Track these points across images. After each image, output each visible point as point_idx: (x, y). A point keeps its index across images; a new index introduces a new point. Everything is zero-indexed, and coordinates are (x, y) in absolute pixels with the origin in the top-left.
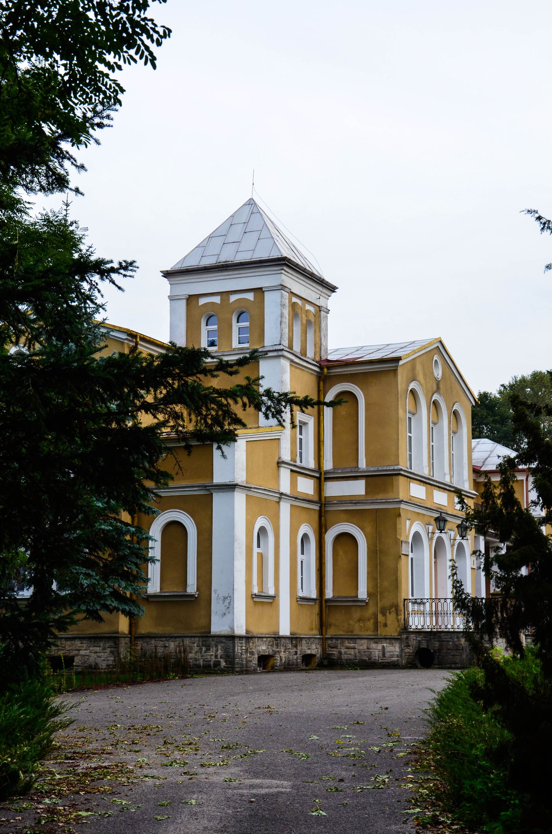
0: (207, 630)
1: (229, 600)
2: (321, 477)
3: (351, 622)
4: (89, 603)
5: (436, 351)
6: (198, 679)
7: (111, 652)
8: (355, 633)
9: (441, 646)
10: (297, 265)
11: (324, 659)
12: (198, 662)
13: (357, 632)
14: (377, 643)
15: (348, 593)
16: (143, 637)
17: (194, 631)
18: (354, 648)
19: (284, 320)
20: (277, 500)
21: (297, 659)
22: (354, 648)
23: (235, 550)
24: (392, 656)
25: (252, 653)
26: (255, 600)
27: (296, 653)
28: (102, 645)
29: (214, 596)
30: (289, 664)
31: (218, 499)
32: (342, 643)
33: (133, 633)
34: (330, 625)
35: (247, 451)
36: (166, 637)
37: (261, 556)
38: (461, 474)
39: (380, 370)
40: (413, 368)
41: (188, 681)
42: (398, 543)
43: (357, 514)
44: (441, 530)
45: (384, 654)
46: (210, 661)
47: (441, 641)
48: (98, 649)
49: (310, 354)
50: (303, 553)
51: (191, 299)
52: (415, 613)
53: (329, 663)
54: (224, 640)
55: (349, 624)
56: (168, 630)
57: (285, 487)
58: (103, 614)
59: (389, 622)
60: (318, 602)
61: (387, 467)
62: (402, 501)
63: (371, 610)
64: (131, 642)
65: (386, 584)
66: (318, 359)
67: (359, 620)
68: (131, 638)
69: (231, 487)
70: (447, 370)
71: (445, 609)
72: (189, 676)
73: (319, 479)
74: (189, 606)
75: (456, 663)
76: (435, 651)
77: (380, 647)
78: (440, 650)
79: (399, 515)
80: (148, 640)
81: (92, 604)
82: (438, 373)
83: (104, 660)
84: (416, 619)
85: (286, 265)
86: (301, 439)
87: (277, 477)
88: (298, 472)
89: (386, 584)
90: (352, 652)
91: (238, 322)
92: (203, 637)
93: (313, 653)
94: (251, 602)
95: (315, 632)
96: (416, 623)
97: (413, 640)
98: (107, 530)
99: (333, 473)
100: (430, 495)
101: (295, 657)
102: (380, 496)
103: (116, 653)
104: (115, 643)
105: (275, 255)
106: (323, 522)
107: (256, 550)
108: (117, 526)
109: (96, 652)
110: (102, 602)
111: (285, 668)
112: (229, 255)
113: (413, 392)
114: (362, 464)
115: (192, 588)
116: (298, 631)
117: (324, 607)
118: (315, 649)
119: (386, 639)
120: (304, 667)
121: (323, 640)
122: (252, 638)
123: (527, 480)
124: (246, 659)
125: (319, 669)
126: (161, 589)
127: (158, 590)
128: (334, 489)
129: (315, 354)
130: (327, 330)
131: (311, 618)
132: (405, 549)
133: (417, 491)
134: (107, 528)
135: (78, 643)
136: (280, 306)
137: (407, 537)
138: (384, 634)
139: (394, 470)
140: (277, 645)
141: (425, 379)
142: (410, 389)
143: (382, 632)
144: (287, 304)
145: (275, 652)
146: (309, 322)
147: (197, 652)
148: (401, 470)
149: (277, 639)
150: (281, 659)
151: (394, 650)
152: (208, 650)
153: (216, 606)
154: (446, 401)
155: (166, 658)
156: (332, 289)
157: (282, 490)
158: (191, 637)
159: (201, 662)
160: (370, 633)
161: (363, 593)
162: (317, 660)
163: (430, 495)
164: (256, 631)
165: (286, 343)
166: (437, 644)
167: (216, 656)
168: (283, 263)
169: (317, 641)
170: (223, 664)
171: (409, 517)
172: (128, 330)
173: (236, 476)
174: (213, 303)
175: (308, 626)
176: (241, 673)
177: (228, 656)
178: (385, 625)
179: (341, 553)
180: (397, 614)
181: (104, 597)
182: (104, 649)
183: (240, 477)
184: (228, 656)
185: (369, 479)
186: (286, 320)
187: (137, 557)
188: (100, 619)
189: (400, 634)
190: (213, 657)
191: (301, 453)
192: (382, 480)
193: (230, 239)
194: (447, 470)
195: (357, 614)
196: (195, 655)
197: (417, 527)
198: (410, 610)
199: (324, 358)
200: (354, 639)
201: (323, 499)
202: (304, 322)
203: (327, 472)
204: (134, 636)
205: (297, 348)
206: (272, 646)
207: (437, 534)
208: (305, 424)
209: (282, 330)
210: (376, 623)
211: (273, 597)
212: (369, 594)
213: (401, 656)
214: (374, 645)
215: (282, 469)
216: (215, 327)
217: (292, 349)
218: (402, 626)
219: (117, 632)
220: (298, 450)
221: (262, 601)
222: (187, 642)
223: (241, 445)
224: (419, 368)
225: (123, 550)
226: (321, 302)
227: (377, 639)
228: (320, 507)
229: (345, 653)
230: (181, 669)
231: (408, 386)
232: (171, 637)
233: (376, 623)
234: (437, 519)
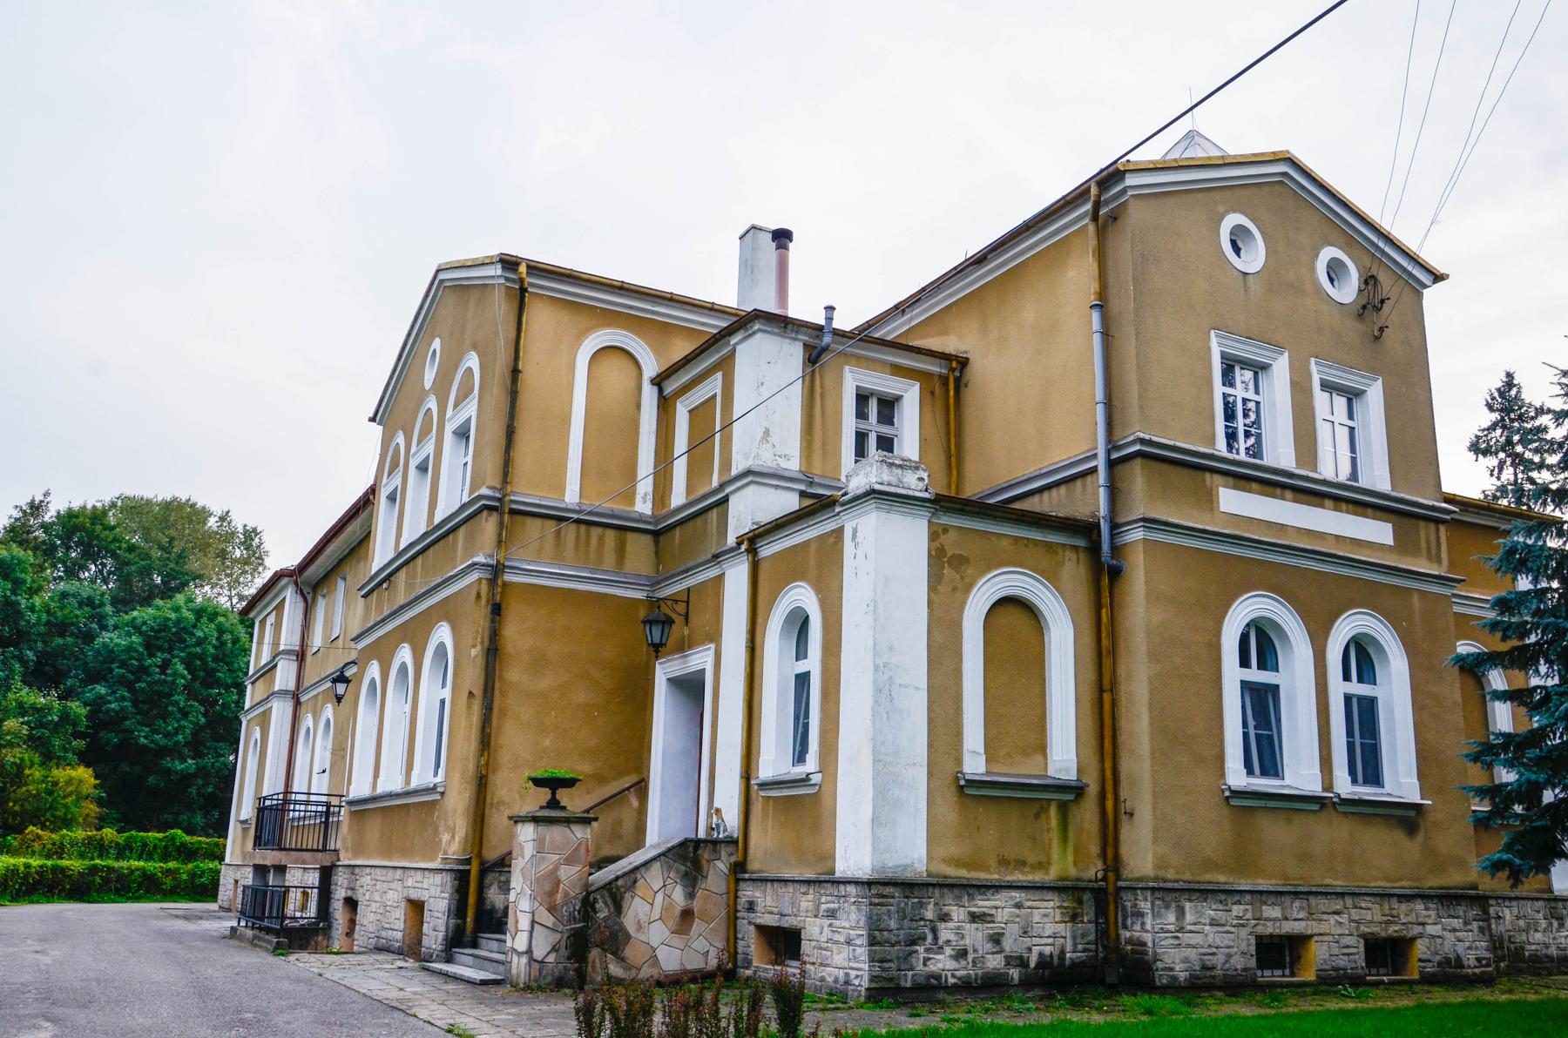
7: (1481, 930)
10: (732, 383)
48: (1456, 923)
83: (1470, 948)
135: (1419, 906)
159: (1553, 951)
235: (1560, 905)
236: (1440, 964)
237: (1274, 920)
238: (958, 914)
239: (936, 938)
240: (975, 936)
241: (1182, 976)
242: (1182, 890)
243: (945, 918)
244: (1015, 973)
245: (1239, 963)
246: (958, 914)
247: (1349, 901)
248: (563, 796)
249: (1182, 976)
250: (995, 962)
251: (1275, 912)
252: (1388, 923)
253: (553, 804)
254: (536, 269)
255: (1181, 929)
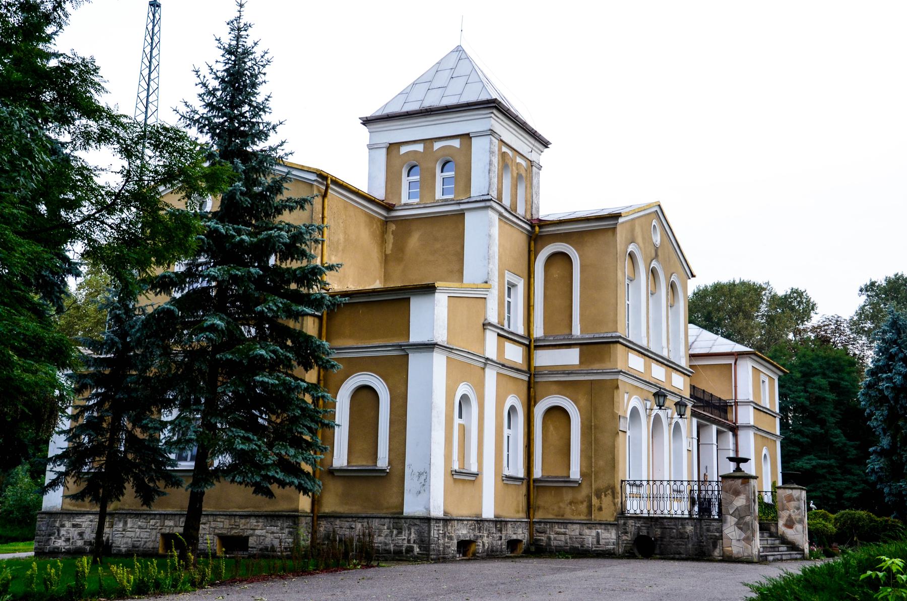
0: (400, 510)
1: (424, 476)
2: (530, 346)
3: (561, 505)
4: (247, 473)
5: (654, 215)
6: (384, 569)
7: (290, 533)
8: (566, 517)
9: (662, 533)
11: (531, 545)
12: (387, 547)
13: (569, 516)
14: (590, 528)
15: (559, 472)
16: (326, 517)
17: (385, 511)
18: (565, 534)
19: (493, 168)
20: (482, 365)
21: (501, 545)
22: (565, 534)
23: (433, 419)
24: (607, 544)
25: (451, 538)
26: (455, 477)
27: (501, 538)
28: (279, 524)
29: (407, 471)
30: (492, 551)
31: (415, 361)
32: (551, 528)
33: (316, 511)
34: (539, 507)
35: (449, 307)
36: (352, 517)
37: (463, 428)
38: (677, 350)
39: (600, 227)
40: (632, 230)
41: (370, 572)
42: (616, 418)
43: (569, 382)
44: (660, 407)
45: (598, 542)
46: (401, 546)
47: (664, 528)
48: (274, 529)
49: (521, 211)
50: (509, 427)
51: (392, 148)
52: (633, 496)
53: (537, 550)
54: (417, 522)
55: (560, 508)
56: (355, 509)
57: (491, 352)
58: (274, 488)
59: (604, 506)
60: (525, 481)
61: (603, 333)
62: (621, 371)
63: (584, 492)
64: (313, 521)
65: (601, 463)
66: (529, 217)
67: (571, 503)
68: (313, 517)
69: (429, 347)
70: (666, 238)
71: (662, 493)
72: (376, 564)
73: (528, 346)
74: (377, 482)
75: (680, 554)
76: (656, 540)
77: (594, 533)
78: (662, 538)
79: (617, 387)
80: (332, 520)
81: (250, 475)
82: (657, 239)
84: (635, 502)
85: (495, 107)
86: (509, 302)
87: (483, 340)
88: (505, 336)
89: (601, 463)
90: (562, 537)
91: (442, 172)
92: (394, 518)
93: (519, 538)
94: (450, 478)
95: (522, 515)
96: (633, 507)
97: (632, 526)
98: (272, 384)
99: (544, 340)
100: (648, 368)
101: (500, 542)
102: (596, 366)
103: (295, 534)
104: (295, 523)
105: (484, 97)
106: (532, 394)
107: (457, 421)
108: (284, 380)
109: (273, 533)
110: (263, 472)
111: (488, 555)
112: (433, 100)
113: (631, 256)
114: (577, 331)
115: (383, 462)
116: (501, 513)
117: (532, 488)
118: (521, 534)
119: (601, 524)
120: (509, 554)
121: (531, 524)
122: (451, 520)
123: (735, 364)
124: (444, 544)
125: (526, 557)
126: (348, 462)
127: (345, 464)
128: (544, 358)
129: (526, 212)
130: (538, 187)
131: (517, 498)
132: (623, 425)
133: (636, 362)
134: (271, 381)
135: (253, 521)
136: (488, 153)
137: (625, 412)
138: (598, 519)
139: (612, 337)
140: (479, 529)
141: (644, 243)
142: (629, 251)
143: (596, 516)
144: (497, 152)
145: (477, 537)
146: (519, 176)
147: (386, 536)
148: (620, 337)
149: (480, 522)
150: (484, 545)
151: (609, 537)
152: (400, 533)
153: (410, 483)
154: (664, 269)
155: (346, 543)
156: (546, 144)
157: (487, 356)
158: (381, 518)
159: (392, 547)
160: (582, 517)
161: (575, 473)
162: (523, 547)
163: (648, 368)
164: (456, 513)
165: (494, 194)
166: (659, 532)
167: (409, 541)
168: (493, 105)
169: (524, 525)
170: (417, 550)
171: (627, 390)
172: (318, 170)
173: (436, 335)
174: (416, 152)
175: (514, 509)
176: (437, 561)
177: (422, 541)
178: (600, 509)
179: (551, 428)
180: (614, 498)
181: (267, 467)
182: (282, 529)
183: (441, 336)
184: (422, 541)
185: (584, 347)
186: (495, 168)
187: (313, 420)
188: (270, 494)
189: (617, 519)
190: (406, 542)
191: (509, 318)
192: (597, 348)
193: (436, 84)
194: (664, 343)
195: (568, 496)
196: (383, 538)
197: (634, 402)
198: (628, 492)
199: (535, 217)
200: (565, 524)
201: (533, 369)
202: (515, 175)
203: (537, 340)
204: (317, 516)
205: (506, 202)
206: (474, 530)
207: (656, 410)
208: (514, 286)
209: (490, 179)
210: (590, 507)
211: (476, 475)
212: (582, 475)
213: (618, 544)
214: (587, 531)
215: (488, 332)
216: (417, 178)
217: (501, 201)
218: (619, 511)
219: (297, 511)
220: (506, 315)
221: (464, 478)
222: (376, 523)
223: (441, 299)
224: (638, 230)
225: (294, 410)
226: (533, 157)
227: (590, 525)
228: (529, 378)
229: (555, 539)
230: (368, 556)
231: (627, 248)
232: (358, 518)
233: (590, 507)
234: (655, 395)
235: (403, 521)
236: (261, 550)
237: (170, 527)
238: (68, 524)
239: (59, 534)
240: (74, 533)
241: (124, 550)
242: (127, 514)
243: (63, 526)
244: (88, 548)
245: (150, 545)
246: (68, 524)
247: (211, 518)
248: (742, 465)
249: (124, 550)
250: (80, 543)
251: (171, 523)
252: (232, 528)
253: (738, 469)
254: (335, 182)
255: (124, 530)
